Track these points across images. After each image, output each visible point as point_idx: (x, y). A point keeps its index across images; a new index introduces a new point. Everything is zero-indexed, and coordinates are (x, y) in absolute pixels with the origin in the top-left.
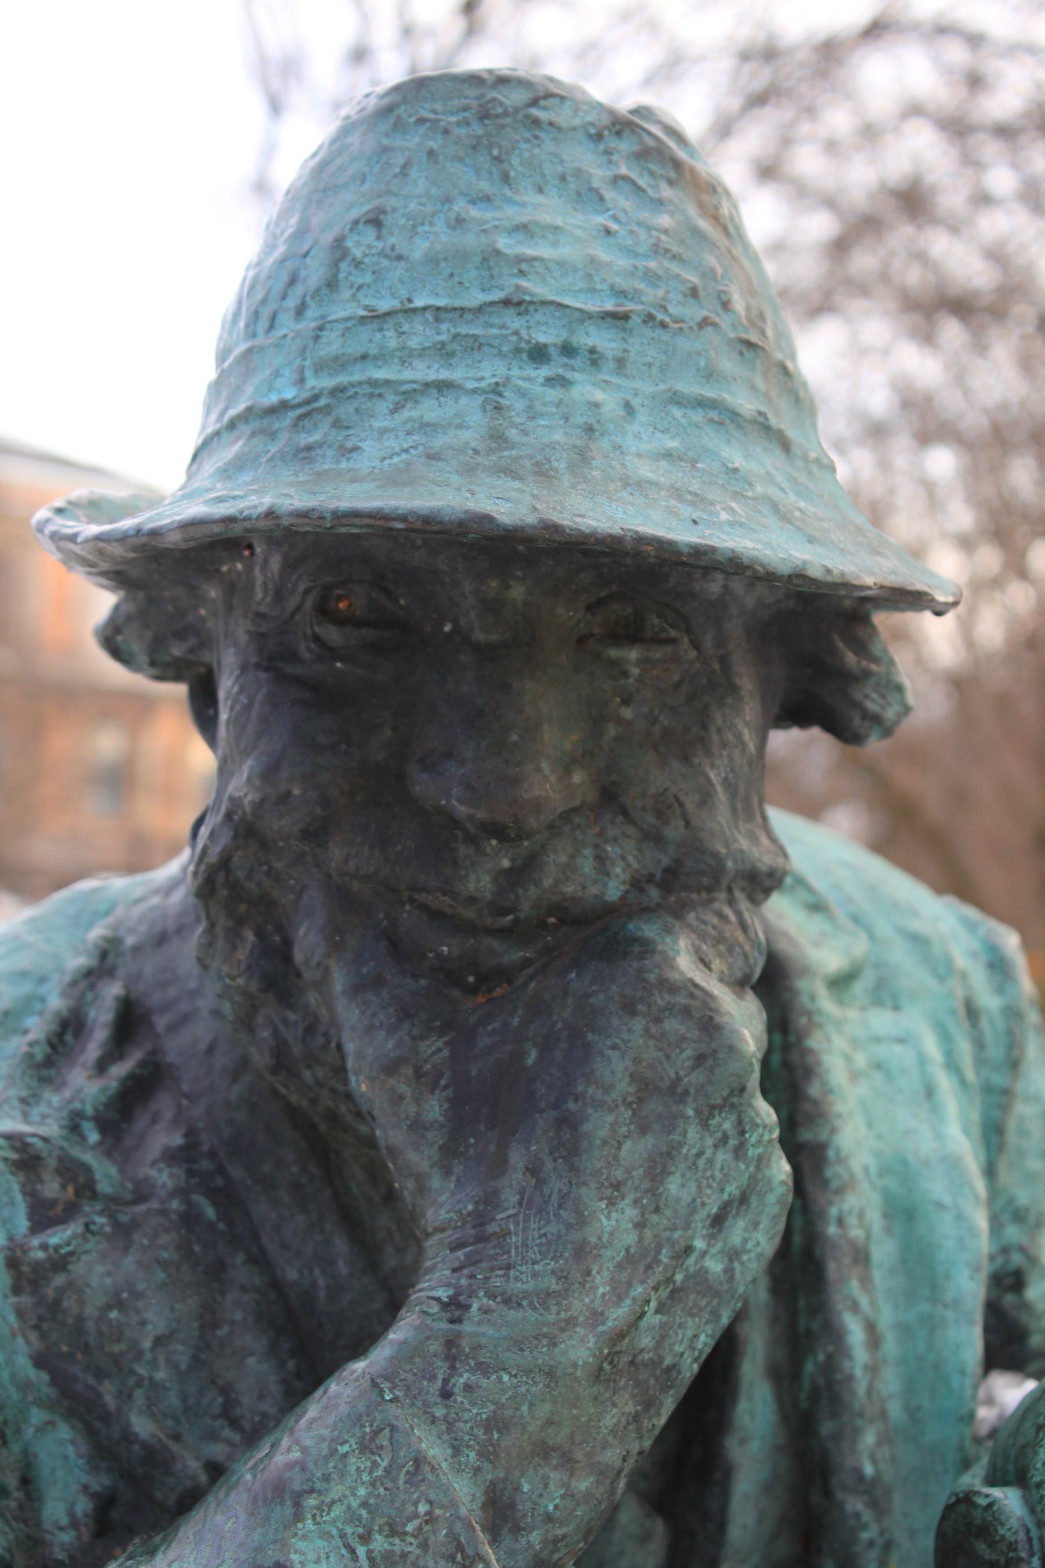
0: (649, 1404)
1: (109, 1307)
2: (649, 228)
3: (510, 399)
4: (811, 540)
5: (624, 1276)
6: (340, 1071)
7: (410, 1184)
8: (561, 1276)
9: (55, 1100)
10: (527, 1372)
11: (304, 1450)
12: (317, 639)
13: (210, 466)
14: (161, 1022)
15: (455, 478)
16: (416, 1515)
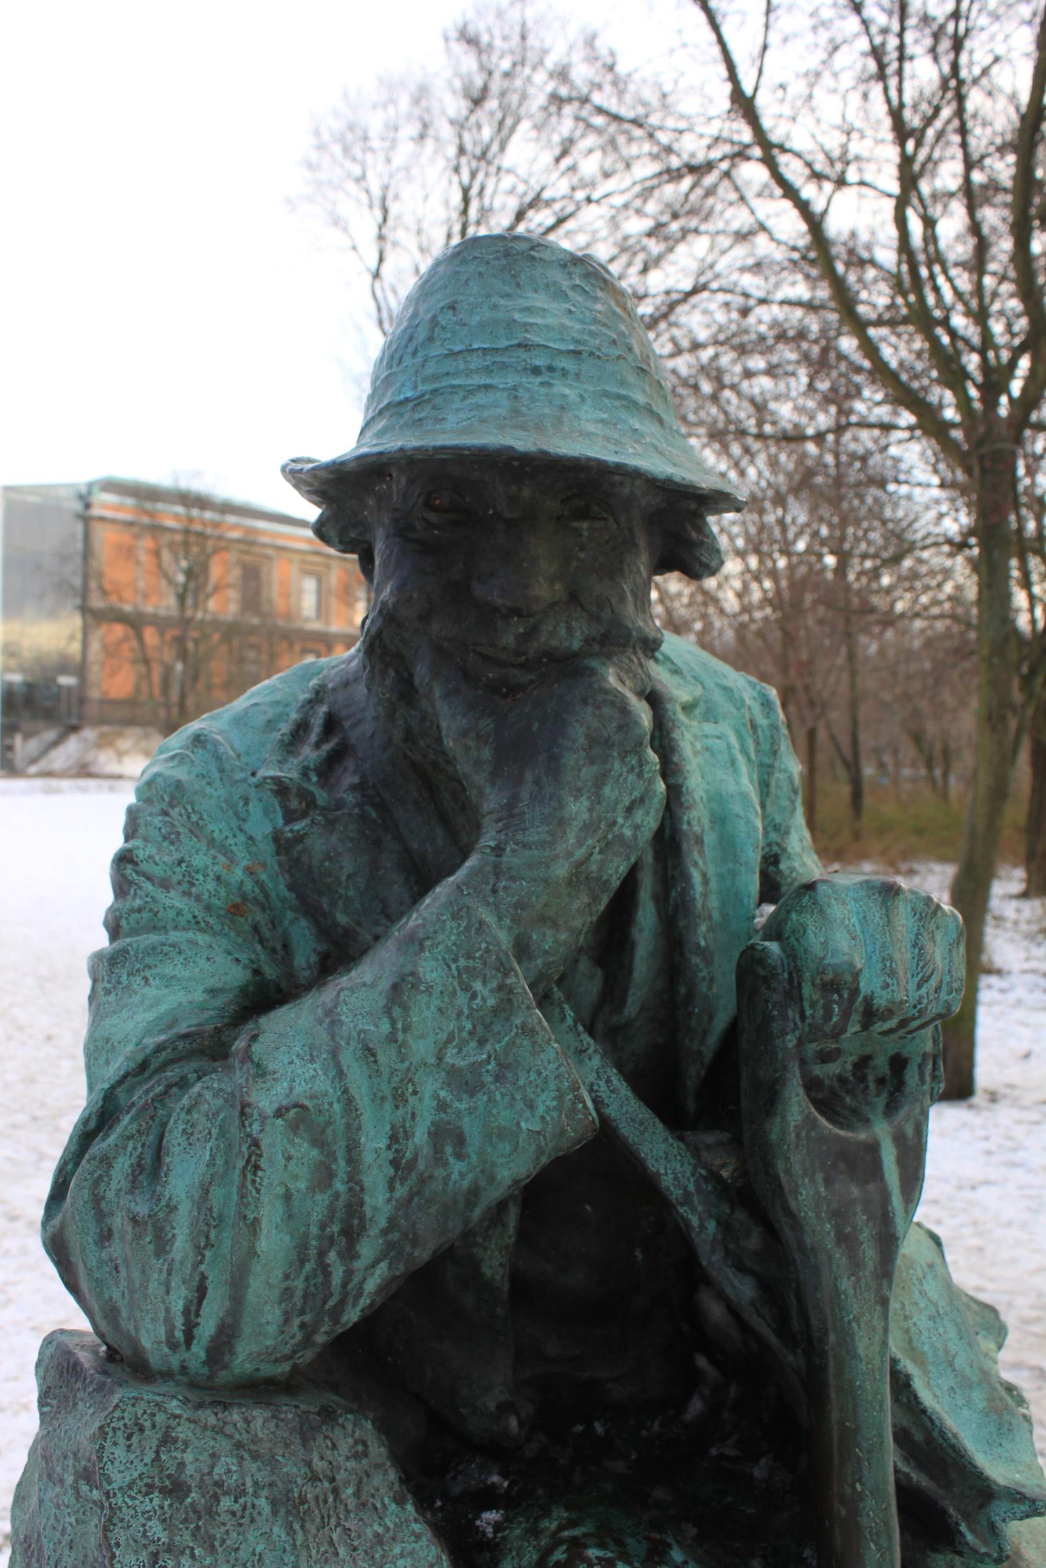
0: (596, 899)
1: (324, 860)
2: (591, 310)
3: (521, 393)
4: (675, 465)
5: (583, 835)
6: (439, 740)
7: (475, 792)
8: (551, 833)
9: (295, 761)
10: (535, 880)
11: (424, 919)
12: (424, 519)
13: (369, 434)
14: (347, 724)
15: (494, 431)
16: (480, 949)
